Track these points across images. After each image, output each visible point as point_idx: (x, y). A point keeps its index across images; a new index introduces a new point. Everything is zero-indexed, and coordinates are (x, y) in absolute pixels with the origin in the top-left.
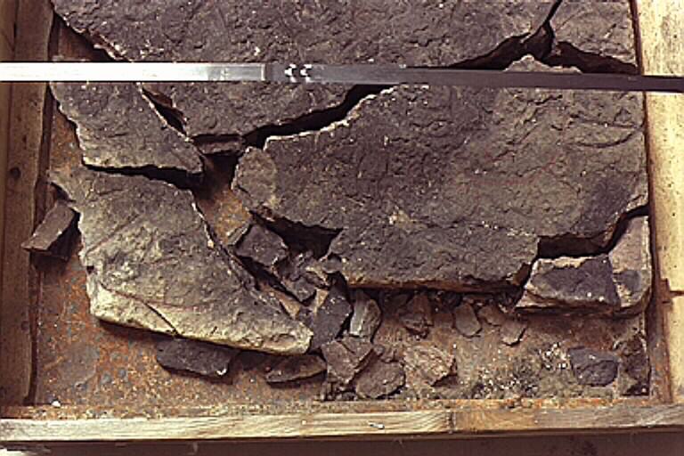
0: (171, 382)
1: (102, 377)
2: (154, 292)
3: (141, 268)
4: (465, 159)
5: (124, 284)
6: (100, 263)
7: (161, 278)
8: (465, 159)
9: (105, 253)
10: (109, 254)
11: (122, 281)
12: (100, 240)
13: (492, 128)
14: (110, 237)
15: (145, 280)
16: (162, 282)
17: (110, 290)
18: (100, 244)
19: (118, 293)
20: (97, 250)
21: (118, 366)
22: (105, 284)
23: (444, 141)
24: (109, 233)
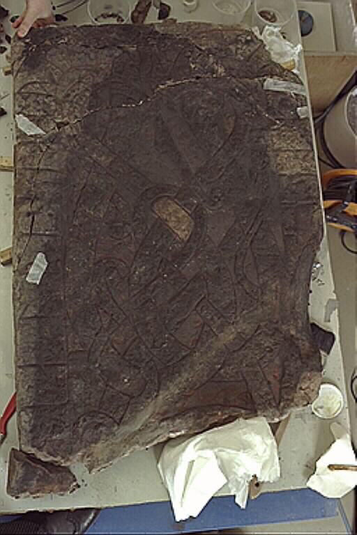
3: (237, 41)
4: (102, 74)
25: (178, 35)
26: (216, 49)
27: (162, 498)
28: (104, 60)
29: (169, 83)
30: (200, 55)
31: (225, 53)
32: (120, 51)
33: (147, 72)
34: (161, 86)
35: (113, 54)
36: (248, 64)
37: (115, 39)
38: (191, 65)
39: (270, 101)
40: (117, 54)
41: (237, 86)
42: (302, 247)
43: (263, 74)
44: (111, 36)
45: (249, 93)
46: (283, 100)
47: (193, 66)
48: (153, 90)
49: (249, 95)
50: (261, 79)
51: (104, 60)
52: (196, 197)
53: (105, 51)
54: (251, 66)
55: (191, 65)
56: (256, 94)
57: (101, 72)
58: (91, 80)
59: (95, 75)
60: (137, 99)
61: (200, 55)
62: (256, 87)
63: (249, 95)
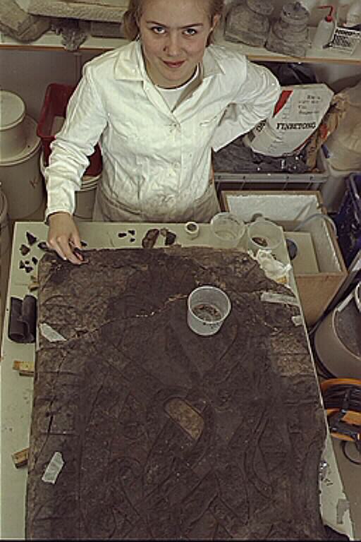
26: (218, 268)
32: (134, 270)
34: (171, 300)
40: (131, 273)
50: (258, 292)
53: (121, 270)
54: (249, 282)
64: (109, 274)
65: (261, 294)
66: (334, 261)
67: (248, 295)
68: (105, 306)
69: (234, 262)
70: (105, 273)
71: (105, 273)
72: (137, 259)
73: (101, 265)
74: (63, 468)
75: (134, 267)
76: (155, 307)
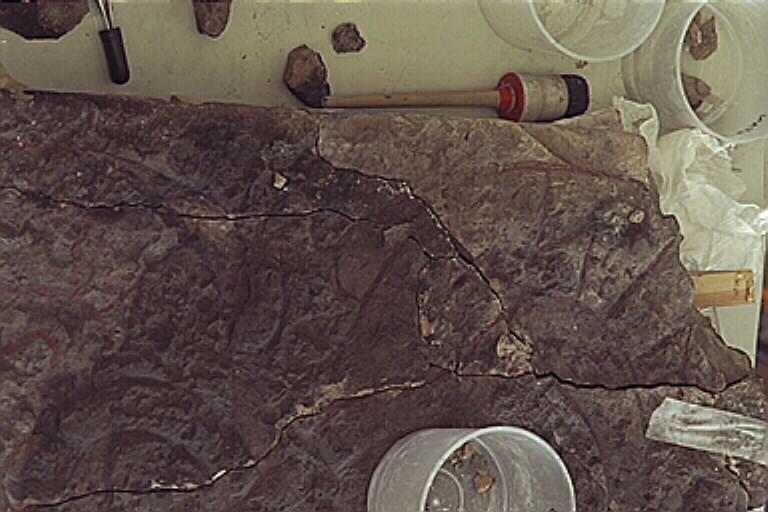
0: (303, 43)
1: (509, 352)
2: (568, 188)
3: (592, 227)
4: (92, 336)
5: (614, 194)
6: (655, 226)
7: (561, 212)
8: (92, 336)
9: (651, 244)
10: (644, 241)
11: (619, 199)
12: (660, 264)
13: (36, 403)
14: (646, 273)
15: (585, 206)
16: (559, 206)
17: (632, 180)
18: (659, 257)
19: (619, 177)
20: (662, 245)
21: (427, 350)
22: (642, 191)
23: (131, 371)
24: (648, 278)
25: (394, 182)
26: (519, 254)
27: (131, 60)
28: (106, 270)
29: (332, 391)
30: (460, 282)
31: (546, 277)
32: (169, 237)
33: (262, 344)
34: (301, 410)
35: (141, 248)
36: (612, 324)
37: (161, 177)
38: (424, 321)
39: (659, 494)
40: (158, 250)
41: (560, 423)
42: (112, 311)
43: (652, 378)
44: (148, 162)
45: (595, 451)
46: (699, 483)
47: (427, 329)
48: (270, 421)
49: (595, 460)
50: (644, 393)
51: (106, 270)
52: (185, 474)
53: (117, 235)
54: (621, 336)
55: (424, 321)
56: (616, 459)
57: (89, 327)
58: (45, 363)
59: (61, 334)
60: (206, 457)
61: (460, 282)
62: (624, 423)
63: (595, 460)
64: (60, 244)
65: (657, 402)
66: (38, 498)
67: (606, 403)
68: (25, 429)
69: (592, 227)
70: (41, 238)
71: (41, 238)
72: (194, 180)
73: (29, 195)
74: (570, 92)
75: (172, 219)
76: (233, 445)
